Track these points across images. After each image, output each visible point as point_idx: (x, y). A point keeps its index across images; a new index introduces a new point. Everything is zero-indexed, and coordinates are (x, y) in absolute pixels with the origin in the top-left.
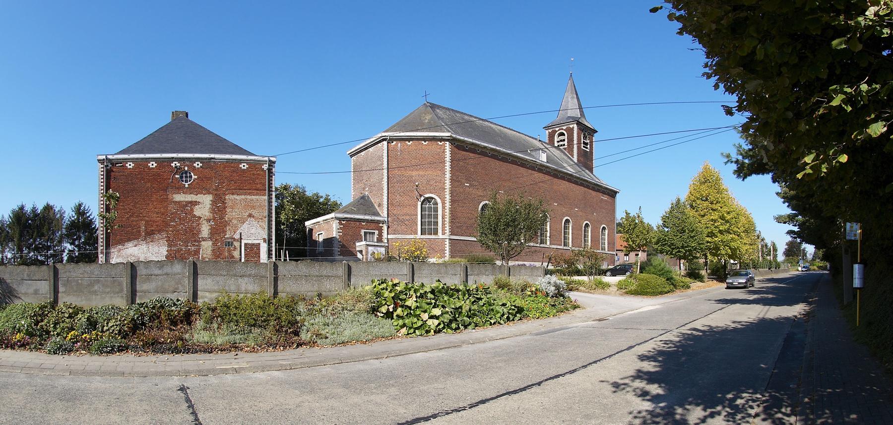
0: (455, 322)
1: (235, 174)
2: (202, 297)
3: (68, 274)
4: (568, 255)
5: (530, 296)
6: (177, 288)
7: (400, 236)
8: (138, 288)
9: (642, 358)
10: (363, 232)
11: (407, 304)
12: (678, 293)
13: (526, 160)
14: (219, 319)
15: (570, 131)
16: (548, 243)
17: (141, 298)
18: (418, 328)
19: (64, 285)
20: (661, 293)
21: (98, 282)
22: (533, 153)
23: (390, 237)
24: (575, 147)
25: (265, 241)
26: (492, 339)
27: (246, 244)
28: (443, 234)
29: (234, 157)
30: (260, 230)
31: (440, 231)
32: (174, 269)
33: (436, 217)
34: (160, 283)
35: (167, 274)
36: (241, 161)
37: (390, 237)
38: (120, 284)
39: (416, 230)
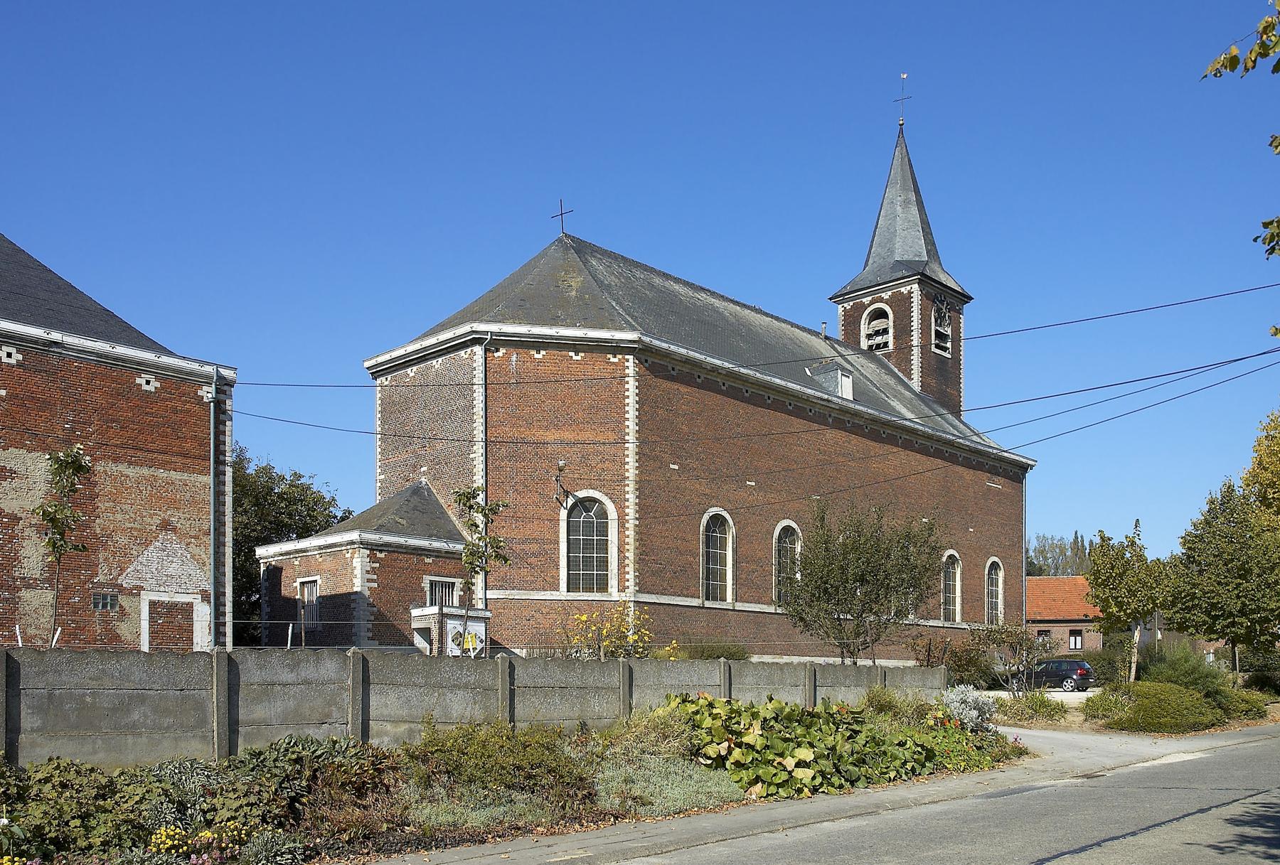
0: (841, 773)
1: (122, 403)
2: (379, 735)
3: (50, 677)
4: (957, 643)
5: (931, 728)
6: (329, 715)
7: (516, 594)
8: (243, 714)
9: (1234, 822)
10: (427, 579)
11: (746, 739)
12: (1235, 727)
13: (807, 399)
14: (445, 778)
15: (901, 303)
16: (958, 618)
17: (249, 738)
18: (779, 786)
19: (38, 710)
20: (1196, 727)
21: (142, 700)
22: (820, 378)
23: (490, 594)
24: (916, 352)
25: (205, 597)
26: (918, 803)
27: (153, 604)
28: (622, 589)
29: (121, 350)
30: (192, 568)
31: (613, 583)
32: (323, 671)
33: (604, 546)
34: (292, 703)
35: (307, 682)
36: (141, 367)
37: (490, 594)
38: (200, 706)
39: (556, 579)
